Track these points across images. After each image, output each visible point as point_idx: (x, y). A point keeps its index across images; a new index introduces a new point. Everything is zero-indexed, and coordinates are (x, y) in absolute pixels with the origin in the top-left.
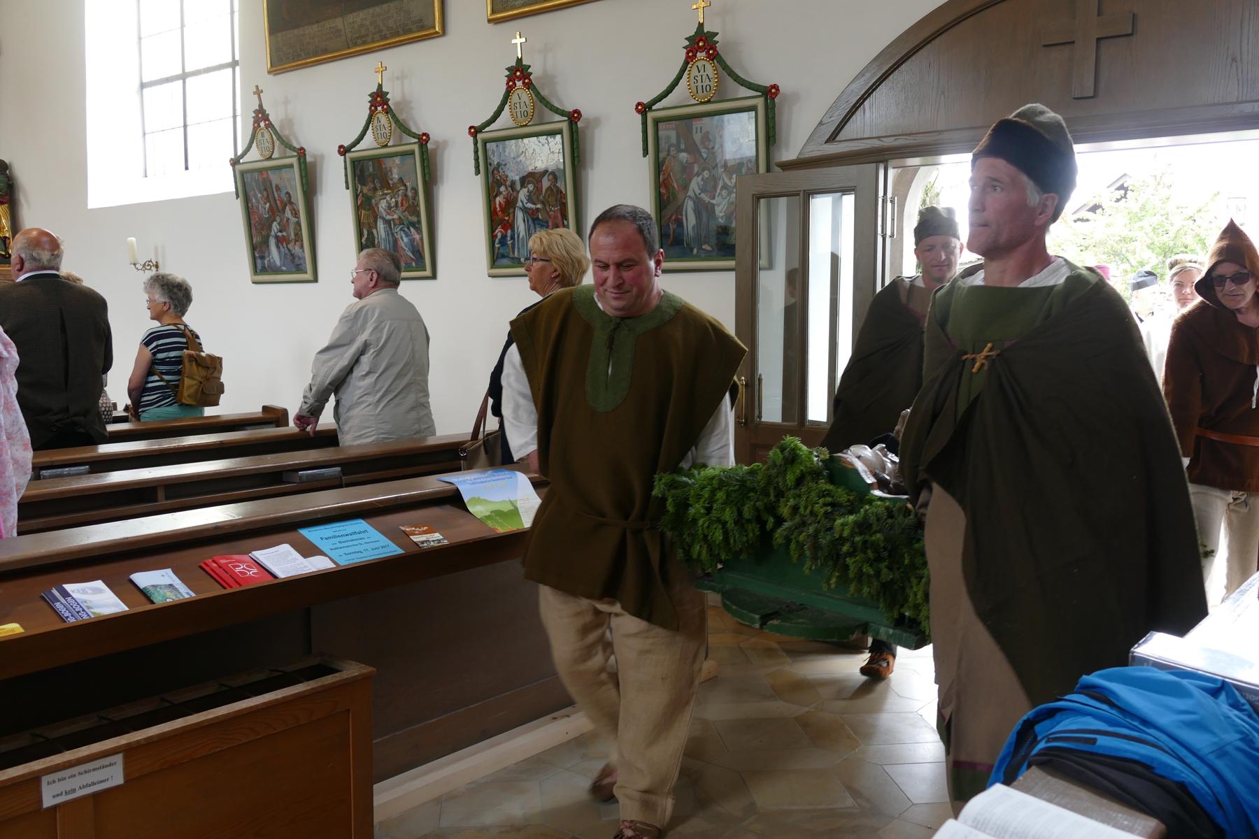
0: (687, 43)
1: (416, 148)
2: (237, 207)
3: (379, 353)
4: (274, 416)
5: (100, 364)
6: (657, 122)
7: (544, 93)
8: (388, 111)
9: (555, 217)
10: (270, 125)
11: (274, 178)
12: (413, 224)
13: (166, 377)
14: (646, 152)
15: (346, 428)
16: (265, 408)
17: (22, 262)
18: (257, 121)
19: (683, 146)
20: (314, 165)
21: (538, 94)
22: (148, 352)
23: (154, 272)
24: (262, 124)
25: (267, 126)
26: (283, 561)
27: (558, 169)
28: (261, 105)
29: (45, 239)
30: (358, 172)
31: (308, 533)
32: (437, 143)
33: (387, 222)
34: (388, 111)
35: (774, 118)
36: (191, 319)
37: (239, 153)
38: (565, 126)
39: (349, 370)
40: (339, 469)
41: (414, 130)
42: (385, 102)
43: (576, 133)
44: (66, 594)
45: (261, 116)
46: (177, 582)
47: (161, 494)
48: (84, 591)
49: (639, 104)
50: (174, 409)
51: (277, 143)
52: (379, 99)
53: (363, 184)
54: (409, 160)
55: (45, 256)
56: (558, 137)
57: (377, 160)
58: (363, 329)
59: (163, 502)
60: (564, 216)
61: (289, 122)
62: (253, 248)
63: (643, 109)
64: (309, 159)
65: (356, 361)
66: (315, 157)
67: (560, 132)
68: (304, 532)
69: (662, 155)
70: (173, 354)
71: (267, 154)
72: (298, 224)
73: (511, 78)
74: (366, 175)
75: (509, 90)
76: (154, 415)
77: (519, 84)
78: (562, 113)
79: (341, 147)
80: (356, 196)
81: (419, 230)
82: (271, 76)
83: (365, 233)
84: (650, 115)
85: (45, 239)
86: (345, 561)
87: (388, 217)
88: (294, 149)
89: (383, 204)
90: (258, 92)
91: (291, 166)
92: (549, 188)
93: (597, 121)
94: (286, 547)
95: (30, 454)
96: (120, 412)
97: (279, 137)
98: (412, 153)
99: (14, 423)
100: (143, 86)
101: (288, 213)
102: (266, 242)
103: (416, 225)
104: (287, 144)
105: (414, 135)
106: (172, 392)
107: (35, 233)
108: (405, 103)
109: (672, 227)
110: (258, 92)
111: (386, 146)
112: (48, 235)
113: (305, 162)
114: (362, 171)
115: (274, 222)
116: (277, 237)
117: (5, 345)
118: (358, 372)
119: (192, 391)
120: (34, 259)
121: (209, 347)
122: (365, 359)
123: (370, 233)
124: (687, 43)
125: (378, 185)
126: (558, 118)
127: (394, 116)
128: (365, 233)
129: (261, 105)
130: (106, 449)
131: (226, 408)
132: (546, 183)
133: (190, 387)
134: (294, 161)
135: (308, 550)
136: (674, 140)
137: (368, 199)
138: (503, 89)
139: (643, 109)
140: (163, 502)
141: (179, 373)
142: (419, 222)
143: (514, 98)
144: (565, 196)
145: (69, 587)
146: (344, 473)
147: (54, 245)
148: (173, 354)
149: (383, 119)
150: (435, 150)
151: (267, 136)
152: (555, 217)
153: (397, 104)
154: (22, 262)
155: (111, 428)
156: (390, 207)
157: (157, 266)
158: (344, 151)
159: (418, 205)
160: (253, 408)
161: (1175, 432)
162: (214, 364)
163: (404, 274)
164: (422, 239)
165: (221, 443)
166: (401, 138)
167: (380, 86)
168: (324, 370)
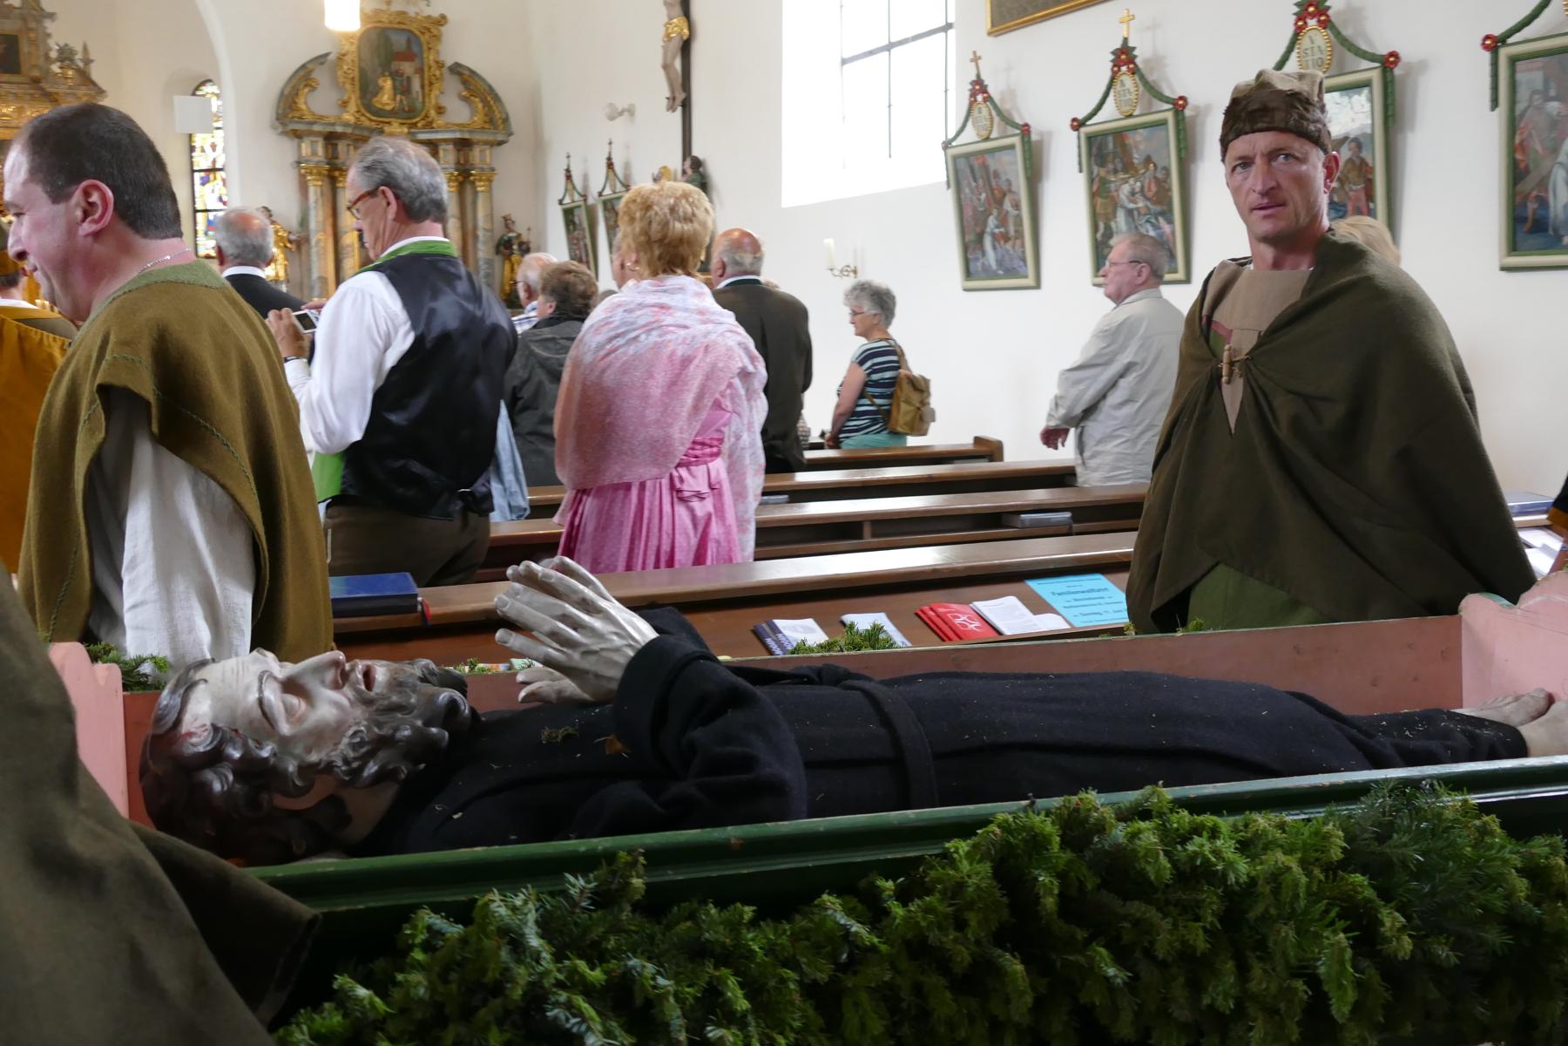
0: (1296, 9)
1: (1170, 116)
2: (947, 200)
3: (1143, 378)
4: (988, 449)
5: (800, 382)
6: (1513, 61)
7: (1347, 32)
8: (1135, 71)
9: (1357, 199)
10: (989, 99)
11: (993, 164)
12: (1162, 214)
13: (878, 401)
14: (1495, 103)
15: (1092, 463)
16: (978, 440)
17: (724, 266)
18: (973, 94)
19: (1552, 93)
20: (1040, 143)
21: (1338, 34)
22: (861, 373)
23: (850, 282)
24: (980, 98)
25: (985, 100)
26: (1007, 614)
27: (1364, 135)
28: (978, 76)
29: (746, 240)
30: (1094, 150)
31: (1039, 587)
32: (1196, 108)
33: (1130, 212)
34: (1135, 71)
35: (1185, 139)
36: (899, 330)
37: (951, 135)
38: (1375, 76)
39: (1103, 396)
40: (1068, 515)
41: (1167, 93)
42: (1131, 60)
43: (1391, 82)
44: (776, 630)
45: (979, 87)
46: (890, 629)
47: (867, 530)
48: (794, 629)
49: (1487, 37)
50: (883, 437)
51: (997, 119)
52: (1124, 57)
53: (1102, 164)
54: (1159, 132)
55: (747, 259)
56: (1366, 91)
57: (1119, 134)
58: (1123, 348)
59: (868, 539)
60: (1370, 197)
61: (1011, 93)
62: (966, 248)
63: (1493, 44)
64: (1034, 137)
65: (1113, 385)
66: (1041, 134)
67: (1367, 84)
68: (1034, 585)
69: (1520, 107)
70: (888, 374)
71: (985, 133)
72: (1019, 219)
73: (1117, 63)
74: (1105, 152)
75: (1298, 32)
76: (855, 443)
77: (1312, 23)
78: (1167, 100)
79: (1074, 120)
80: (1091, 181)
81: (1170, 222)
82: (991, 39)
83: (1102, 226)
84: (1504, 53)
85: (746, 240)
86: (1081, 623)
87: (1132, 206)
88: (1015, 126)
89: (1126, 189)
90: (976, 59)
91: (1012, 147)
92: (1350, 161)
93: (1422, 66)
94: (1012, 600)
95: (762, 476)
96: (815, 438)
97: (999, 112)
98: (1164, 123)
99: (752, 445)
100: (844, 62)
101: (1007, 205)
102: (980, 238)
103: (1167, 214)
104: (1007, 120)
105: (1167, 100)
106: (883, 419)
107: (736, 234)
108: (1157, 61)
109: (1532, 206)
110: (976, 59)
111: (1131, 116)
112: (749, 235)
113: (1029, 142)
114: (1100, 148)
115: (992, 221)
116: (993, 235)
117: (752, 359)
118: (1114, 398)
119: (908, 418)
120: (737, 263)
121: (917, 365)
122: (1124, 384)
123: (1108, 228)
124: (1296, 9)
125: (1119, 166)
126: (1366, 64)
127: (1142, 77)
128: (1102, 226)
129: (978, 76)
130: (803, 478)
131: (938, 437)
132: (1345, 154)
133: (907, 413)
134: (1016, 140)
135: (1038, 606)
136: (1539, 85)
137: (1104, 182)
138: (1289, 31)
139: (1493, 44)
140: (868, 539)
141: (890, 396)
142: (1170, 210)
143: (1305, 42)
144: (1371, 170)
145: (780, 623)
146: (1075, 519)
147: (755, 246)
148: (888, 374)
149: (1128, 81)
150: (1194, 118)
151: (985, 112)
152: (1357, 199)
153: (1147, 61)
154: (724, 266)
155: (809, 455)
156: (1133, 193)
157: (855, 272)
158: (1077, 124)
159: (1170, 190)
160: (962, 439)
161: (31, 493)
162: (920, 387)
163: (1168, 277)
164: (1173, 233)
165: (930, 477)
166: (1150, 104)
167: (1126, 40)
168: (1074, 392)
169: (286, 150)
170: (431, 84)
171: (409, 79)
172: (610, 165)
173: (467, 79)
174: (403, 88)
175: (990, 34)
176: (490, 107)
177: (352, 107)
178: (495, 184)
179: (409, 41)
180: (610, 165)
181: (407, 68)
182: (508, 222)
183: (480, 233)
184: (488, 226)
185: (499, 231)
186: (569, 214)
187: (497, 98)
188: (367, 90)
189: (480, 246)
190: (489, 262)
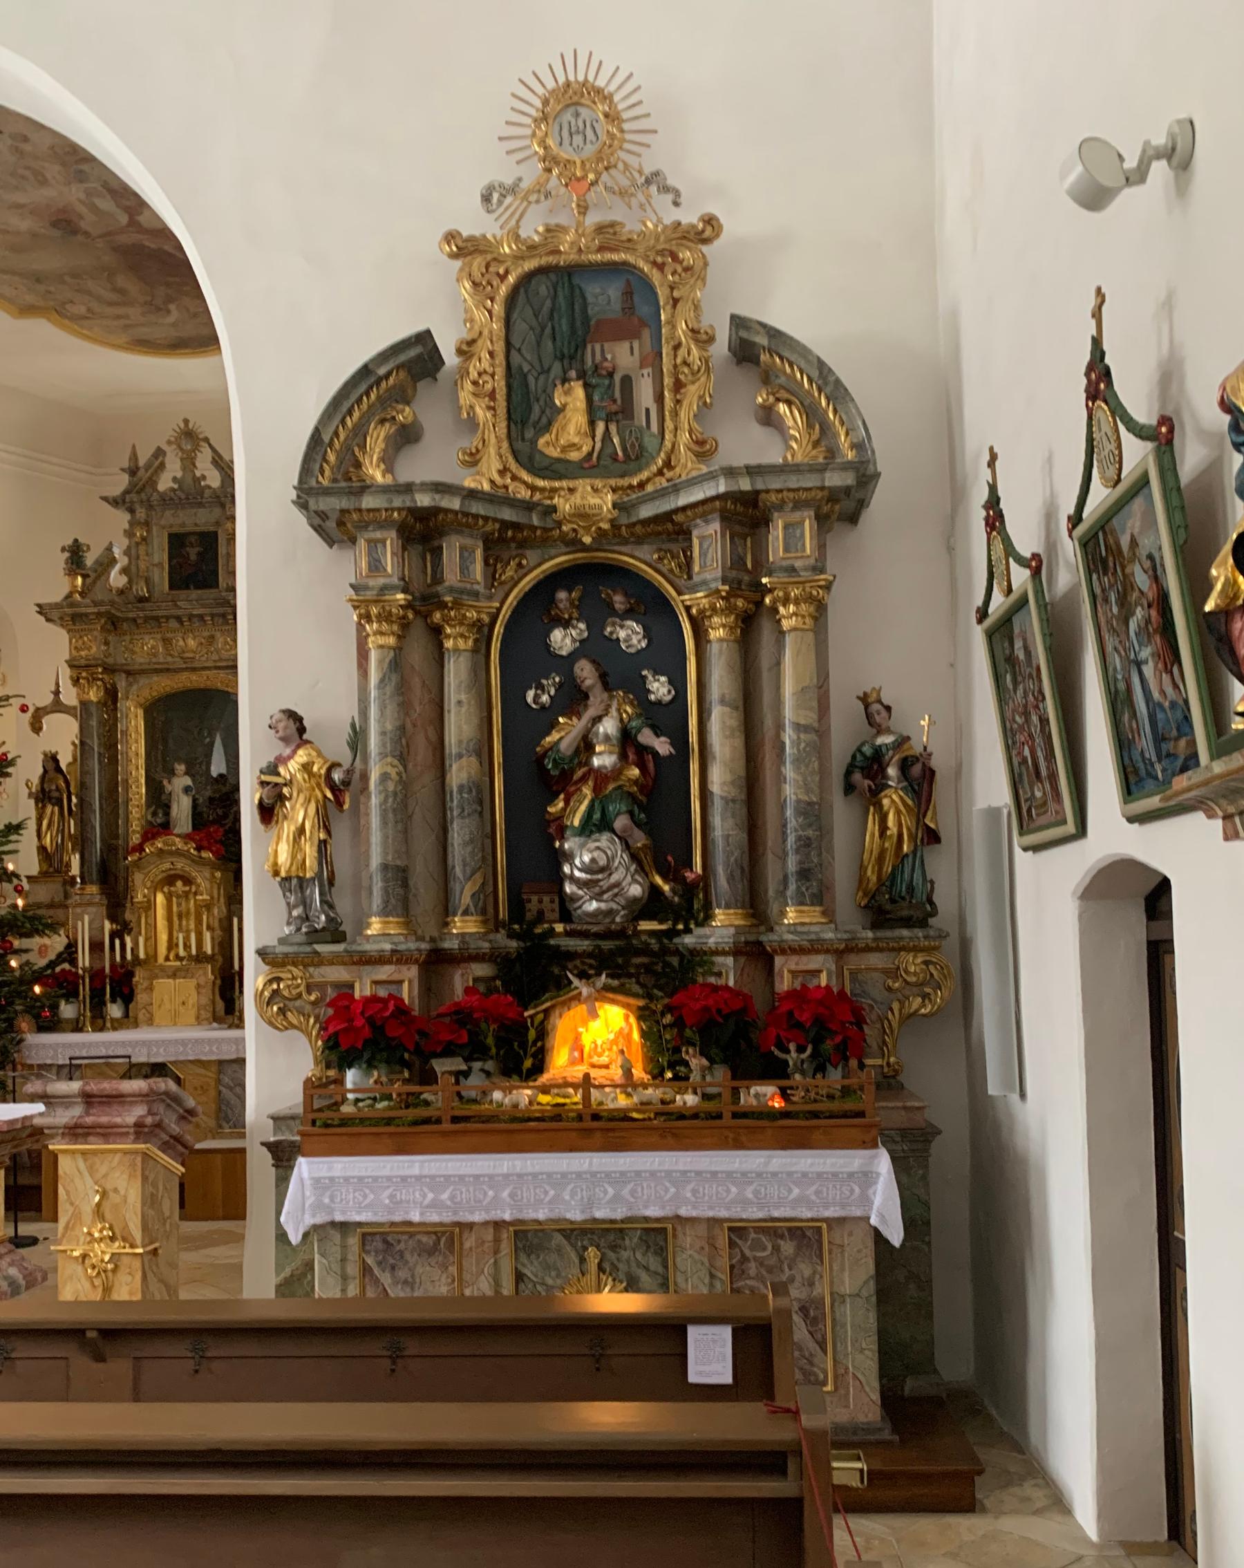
82: (941, 1127)
169: (346, 566)
170: (678, 386)
171: (627, 381)
172: (1099, 380)
173: (755, 349)
174: (610, 402)
175: (939, 1132)
176: (825, 428)
177: (491, 465)
178: (836, 604)
179: (628, 294)
180: (1099, 380)
181: (623, 356)
182: (873, 709)
183: (788, 736)
184: (810, 718)
185: (845, 734)
186: (1001, 633)
187: (838, 393)
188: (525, 412)
189: (789, 771)
190: (814, 813)
